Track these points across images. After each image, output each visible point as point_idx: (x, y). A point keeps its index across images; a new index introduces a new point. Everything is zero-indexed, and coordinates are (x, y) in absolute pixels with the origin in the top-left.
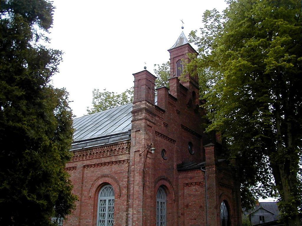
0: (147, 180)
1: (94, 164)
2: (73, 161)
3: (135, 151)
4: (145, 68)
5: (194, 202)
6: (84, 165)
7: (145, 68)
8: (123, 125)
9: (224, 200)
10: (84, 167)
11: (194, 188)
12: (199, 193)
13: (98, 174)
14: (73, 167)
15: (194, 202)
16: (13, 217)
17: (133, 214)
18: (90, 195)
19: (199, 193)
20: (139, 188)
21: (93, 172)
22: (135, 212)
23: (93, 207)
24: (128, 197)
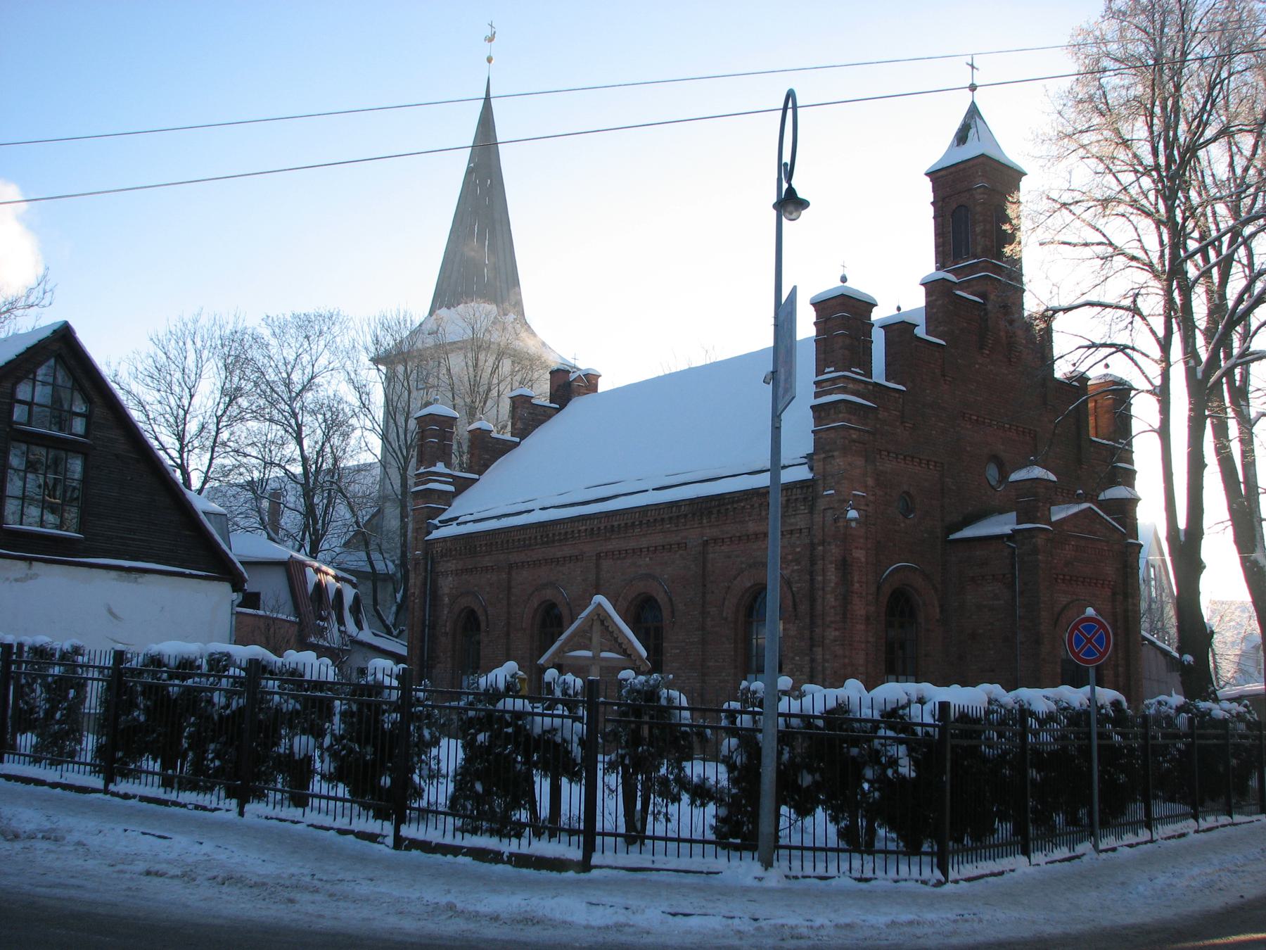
0: (856, 579)
1: (731, 538)
2: (676, 529)
3: (825, 509)
4: (844, 279)
5: (990, 627)
6: (705, 538)
7: (844, 279)
8: (668, 875)
9: (240, 817)
10: (706, 543)
11: (990, 588)
12: (1002, 602)
13: (742, 563)
14: (678, 544)
15: (990, 627)
16: (1042, 774)
17: (824, 660)
18: (724, 615)
19: (1002, 602)
20: (836, 600)
21: (729, 557)
22: (828, 657)
23: (733, 645)
24: (812, 616)
